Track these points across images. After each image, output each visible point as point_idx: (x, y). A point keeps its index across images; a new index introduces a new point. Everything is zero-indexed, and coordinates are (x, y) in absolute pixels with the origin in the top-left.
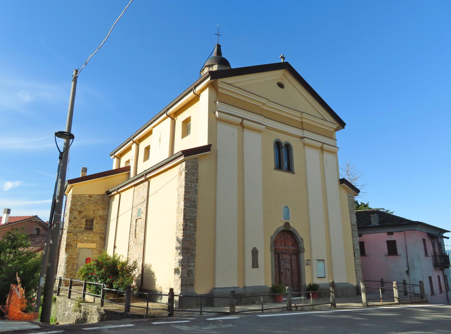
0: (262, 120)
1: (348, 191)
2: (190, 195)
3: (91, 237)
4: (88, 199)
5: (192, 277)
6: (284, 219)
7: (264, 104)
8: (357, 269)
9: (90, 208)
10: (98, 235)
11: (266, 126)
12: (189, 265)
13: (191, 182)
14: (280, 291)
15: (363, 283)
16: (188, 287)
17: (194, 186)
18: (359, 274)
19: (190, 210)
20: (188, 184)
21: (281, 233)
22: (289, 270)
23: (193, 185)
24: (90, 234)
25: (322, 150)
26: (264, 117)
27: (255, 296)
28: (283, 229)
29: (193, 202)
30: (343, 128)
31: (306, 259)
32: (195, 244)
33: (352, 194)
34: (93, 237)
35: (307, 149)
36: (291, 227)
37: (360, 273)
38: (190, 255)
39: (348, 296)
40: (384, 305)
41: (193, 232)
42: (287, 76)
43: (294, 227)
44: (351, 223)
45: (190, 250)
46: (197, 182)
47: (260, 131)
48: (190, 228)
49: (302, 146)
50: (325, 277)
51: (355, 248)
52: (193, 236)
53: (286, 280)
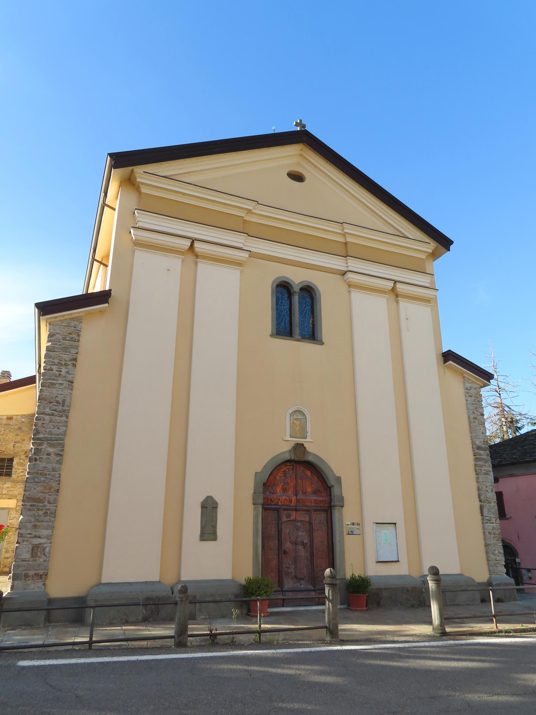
0: (243, 241)
1: (464, 377)
2: (54, 391)
3: (8, 487)
4: (5, 423)
5: (42, 560)
6: (291, 437)
7: (249, 211)
8: (488, 544)
9: (9, 438)
10: (21, 484)
11: (250, 251)
12: (37, 534)
13: (60, 364)
14: (256, 591)
15: (433, 576)
16: (29, 580)
17: (66, 373)
18: (494, 554)
19: (51, 421)
20: (51, 370)
21: (288, 467)
22: (304, 545)
23: (64, 370)
24: (6, 484)
25: (397, 296)
26: (247, 235)
27: (196, 603)
28: (287, 457)
29: (60, 403)
30: (446, 250)
31: (347, 521)
32: (58, 491)
33: (475, 382)
34: (12, 489)
35: (357, 296)
36: (308, 452)
37: (497, 552)
38: (41, 513)
39: (458, 605)
40: (501, 631)
41: (54, 465)
42: (310, 159)
43: (317, 454)
44: (473, 443)
45: (44, 502)
46: (74, 365)
47: (238, 264)
48: (48, 457)
49: (347, 287)
50: (398, 561)
51: (482, 497)
52: (54, 473)
53: (296, 568)
